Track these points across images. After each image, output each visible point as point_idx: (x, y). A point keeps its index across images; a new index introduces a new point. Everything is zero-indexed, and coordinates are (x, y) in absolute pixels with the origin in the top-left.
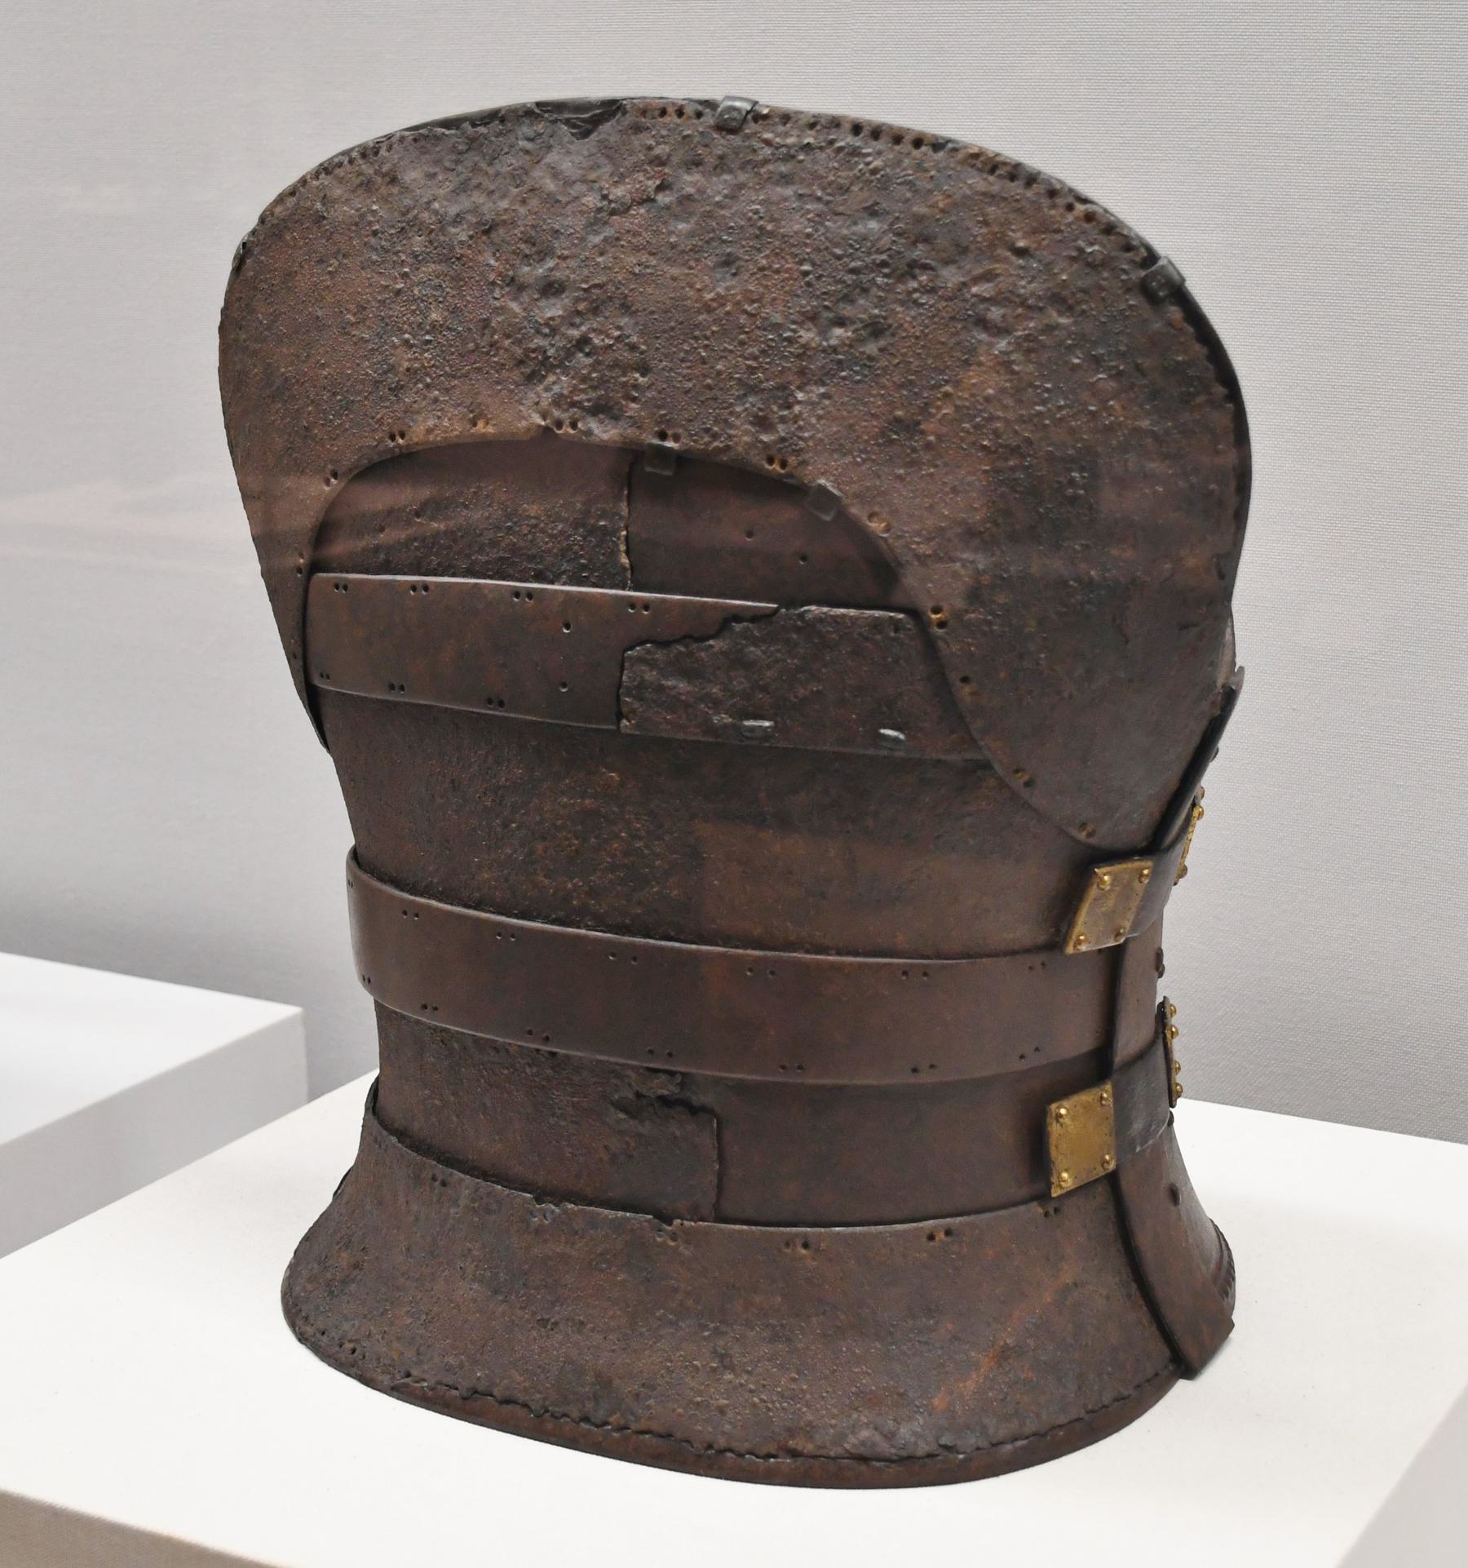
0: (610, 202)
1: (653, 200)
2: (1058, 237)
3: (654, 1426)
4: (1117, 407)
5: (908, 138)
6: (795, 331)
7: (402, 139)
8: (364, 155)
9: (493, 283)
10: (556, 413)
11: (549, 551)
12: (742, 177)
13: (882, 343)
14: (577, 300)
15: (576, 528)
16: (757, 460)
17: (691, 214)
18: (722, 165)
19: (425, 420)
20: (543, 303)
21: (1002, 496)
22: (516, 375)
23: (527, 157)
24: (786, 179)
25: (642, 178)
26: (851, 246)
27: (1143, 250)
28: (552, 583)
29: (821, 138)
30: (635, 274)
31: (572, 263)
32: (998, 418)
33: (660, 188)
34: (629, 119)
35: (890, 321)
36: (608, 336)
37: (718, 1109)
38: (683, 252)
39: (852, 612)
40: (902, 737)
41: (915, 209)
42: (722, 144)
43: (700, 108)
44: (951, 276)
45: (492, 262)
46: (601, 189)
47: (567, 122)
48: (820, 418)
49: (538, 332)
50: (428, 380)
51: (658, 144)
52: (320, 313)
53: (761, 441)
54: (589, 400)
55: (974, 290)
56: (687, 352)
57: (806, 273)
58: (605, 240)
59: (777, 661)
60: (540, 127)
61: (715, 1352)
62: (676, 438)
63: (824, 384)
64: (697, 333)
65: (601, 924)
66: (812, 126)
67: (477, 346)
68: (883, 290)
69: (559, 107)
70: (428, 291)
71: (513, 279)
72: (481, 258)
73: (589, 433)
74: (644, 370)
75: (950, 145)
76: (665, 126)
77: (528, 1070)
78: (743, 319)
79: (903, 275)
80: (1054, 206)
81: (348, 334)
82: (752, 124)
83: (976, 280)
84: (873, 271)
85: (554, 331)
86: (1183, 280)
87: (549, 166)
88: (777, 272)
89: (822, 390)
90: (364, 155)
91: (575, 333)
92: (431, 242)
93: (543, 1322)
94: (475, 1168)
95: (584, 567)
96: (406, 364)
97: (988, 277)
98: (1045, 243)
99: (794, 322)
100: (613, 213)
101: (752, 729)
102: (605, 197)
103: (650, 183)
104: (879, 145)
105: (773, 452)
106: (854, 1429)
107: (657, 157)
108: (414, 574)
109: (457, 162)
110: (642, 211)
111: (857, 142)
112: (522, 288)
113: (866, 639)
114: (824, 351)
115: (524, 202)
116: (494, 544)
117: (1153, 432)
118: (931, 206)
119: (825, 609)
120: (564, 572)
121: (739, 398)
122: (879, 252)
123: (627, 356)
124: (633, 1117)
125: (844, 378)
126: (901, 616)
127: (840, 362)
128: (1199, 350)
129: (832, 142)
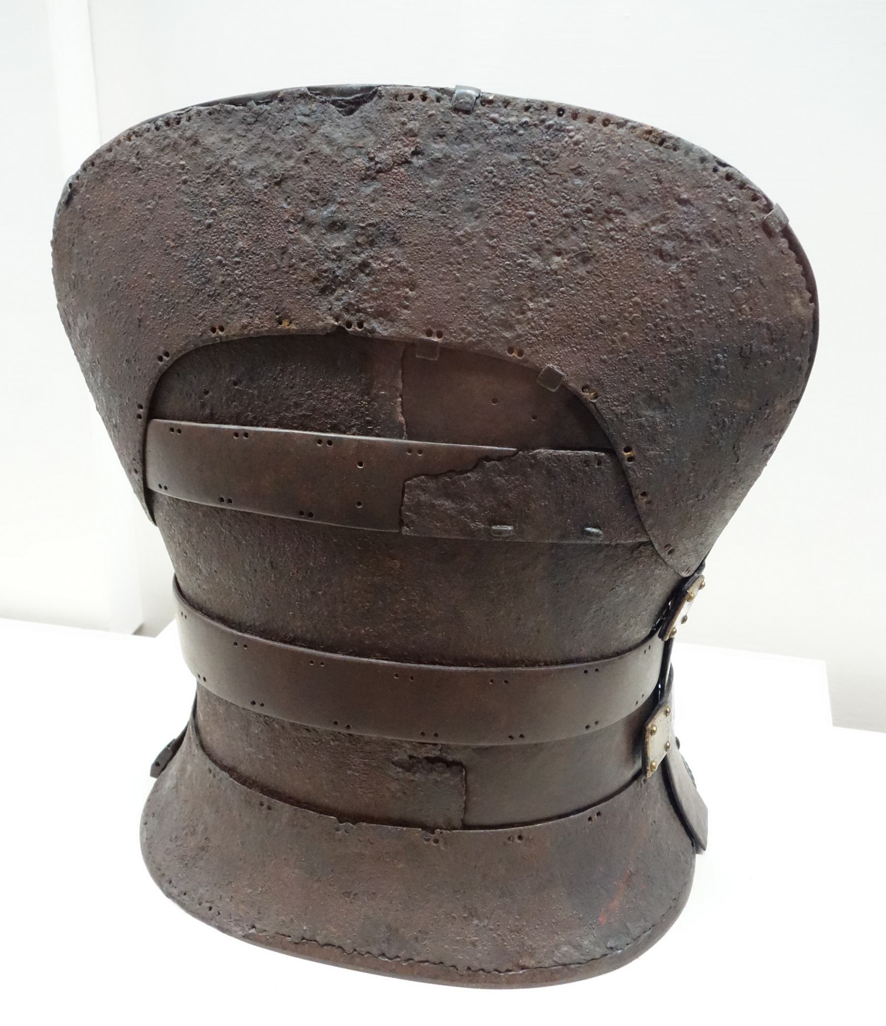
0: (377, 163)
1: (410, 162)
2: (709, 191)
3: (431, 958)
4: (747, 309)
5: (599, 119)
6: (525, 259)
7: (199, 113)
8: (167, 124)
9: (288, 221)
10: (347, 317)
11: (342, 411)
12: (478, 146)
13: (589, 267)
14: (357, 235)
15: (362, 396)
16: (500, 349)
17: (441, 173)
18: (461, 137)
19: (240, 319)
20: (328, 237)
21: (674, 371)
22: (312, 289)
23: (305, 128)
24: (510, 148)
25: (400, 146)
26: (563, 197)
27: (764, 199)
28: (345, 433)
29: (535, 117)
30: (401, 217)
31: (350, 208)
32: (671, 319)
33: (415, 153)
34: (384, 102)
35: (595, 252)
36: (383, 261)
37: (465, 763)
38: (436, 201)
39: (569, 453)
40: (601, 532)
41: (609, 171)
42: (459, 121)
43: (439, 94)
44: (635, 220)
45: (285, 205)
46: (368, 153)
47: (334, 103)
48: (546, 320)
49: (327, 258)
50: (240, 290)
51: (410, 120)
52: (143, 238)
53: (504, 337)
54: (371, 308)
55: (653, 229)
56: (444, 273)
57: (531, 217)
58: (375, 191)
59: (516, 486)
60: (314, 106)
61: (465, 907)
62: (439, 335)
63: (548, 297)
64: (452, 260)
65: (385, 655)
66: (527, 109)
67: (279, 268)
68: (589, 229)
69: (326, 91)
70: (235, 226)
71: (303, 219)
72: (275, 202)
73: (373, 331)
74: (413, 286)
75: (630, 124)
76: (413, 106)
77: (332, 743)
78: (486, 250)
79: (603, 218)
80: (705, 169)
81: (169, 254)
82: (481, 107)
83: (654, 222)
84: (581, 215)
85: (340, 258)
86: (788, 221)
87: (323, 135)
88: (510, 216)
89: (547, 301)
90: (167, 124)
91: (357, 259)
92: (233, 190)
93: (347, 894)
94: (290, 798)
95: (369, 423)
96: (221, 279)
97: (664, 219)
98: (700, 195)
99: (524, 253)
100: (379, 171)
101: (500, 532)
102: (372, 159)
103: (406, 149)
104: (578, 123)
105: (513, 344)
106: (557, 947)
107: (411, 130)
108: (234, 424)
109: (247, 131)
110: (402, 170)
111: (562, 121)
112: (311, 225)
113: (579, 470)
114: (547, 273)
115: (306, 162)
116: (297, 405)
117: (768, 325)
118: (619, 169)
119: (551, 451)
120: (353, 426)
121: (486, 306)
122: (584, 201)
123: (400, 277)
124: (408, 770)
125: (562, 292)
126: (603, 454)
127: (559, 281)
128: (798, 268)
129: (543, 121)
